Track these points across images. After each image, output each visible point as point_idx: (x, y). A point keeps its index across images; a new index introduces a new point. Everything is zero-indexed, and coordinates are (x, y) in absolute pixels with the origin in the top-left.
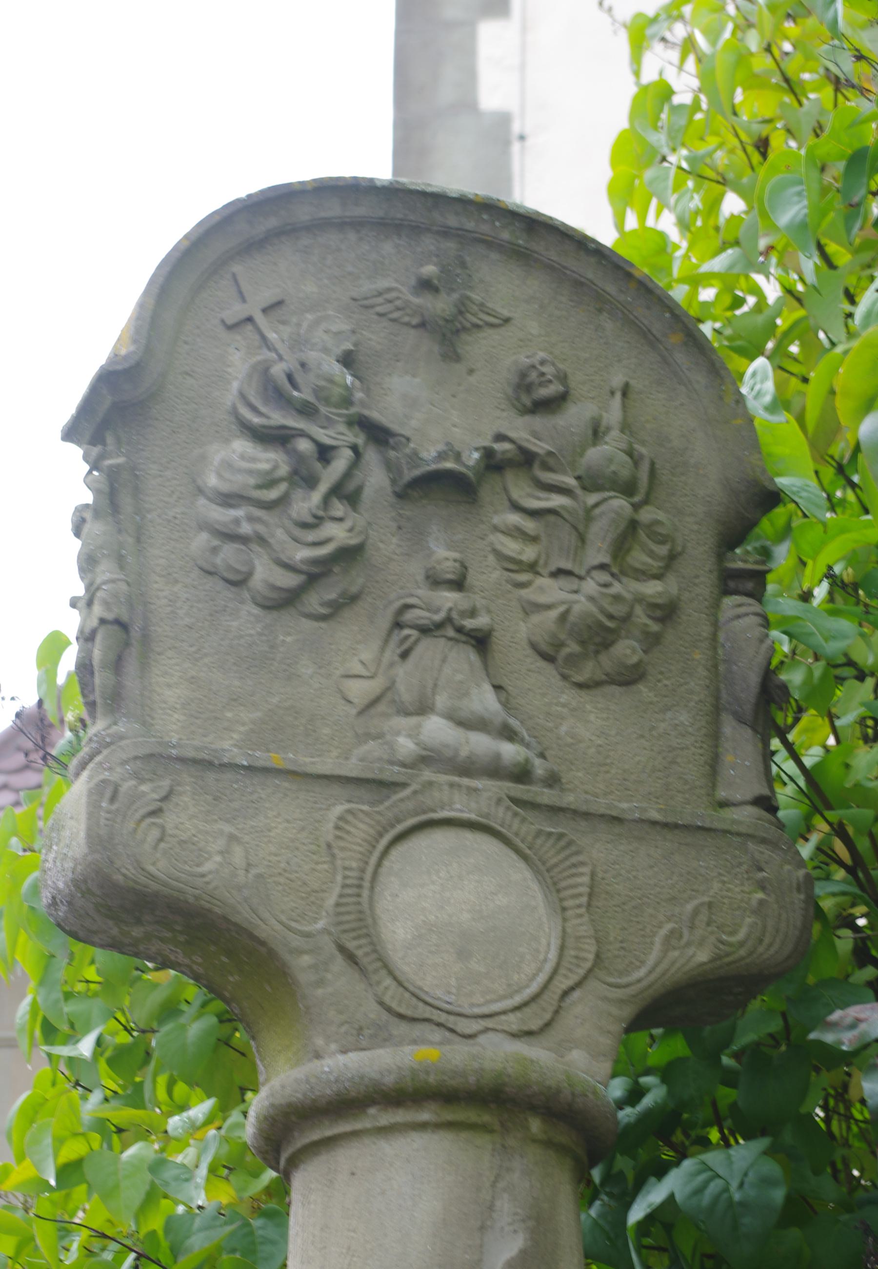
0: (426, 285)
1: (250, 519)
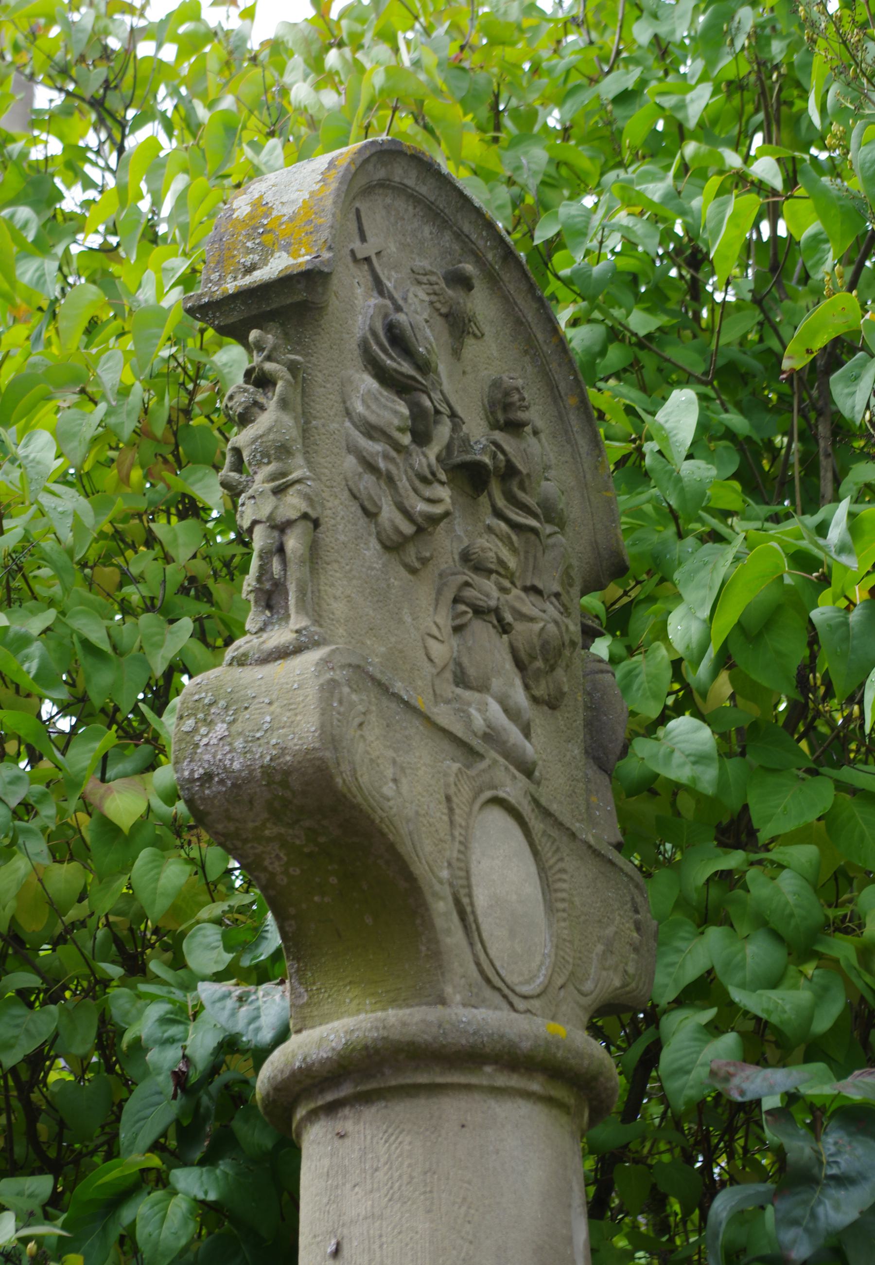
1: (386, 457)
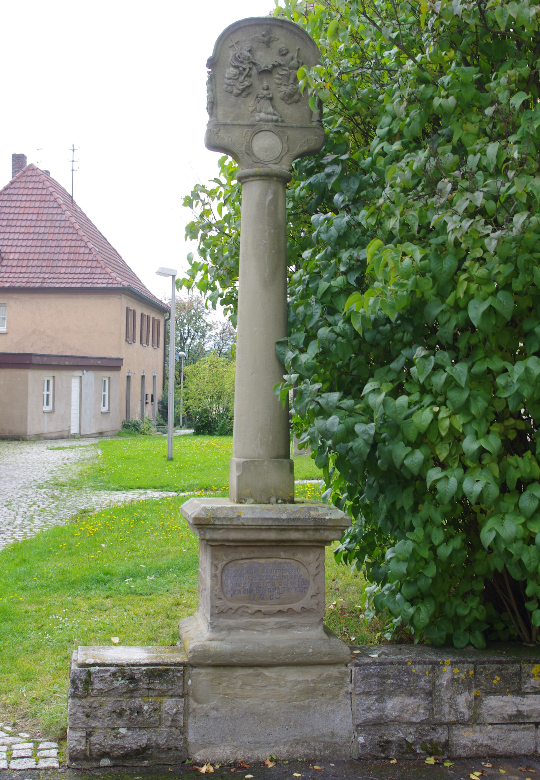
0: (263, 36)
